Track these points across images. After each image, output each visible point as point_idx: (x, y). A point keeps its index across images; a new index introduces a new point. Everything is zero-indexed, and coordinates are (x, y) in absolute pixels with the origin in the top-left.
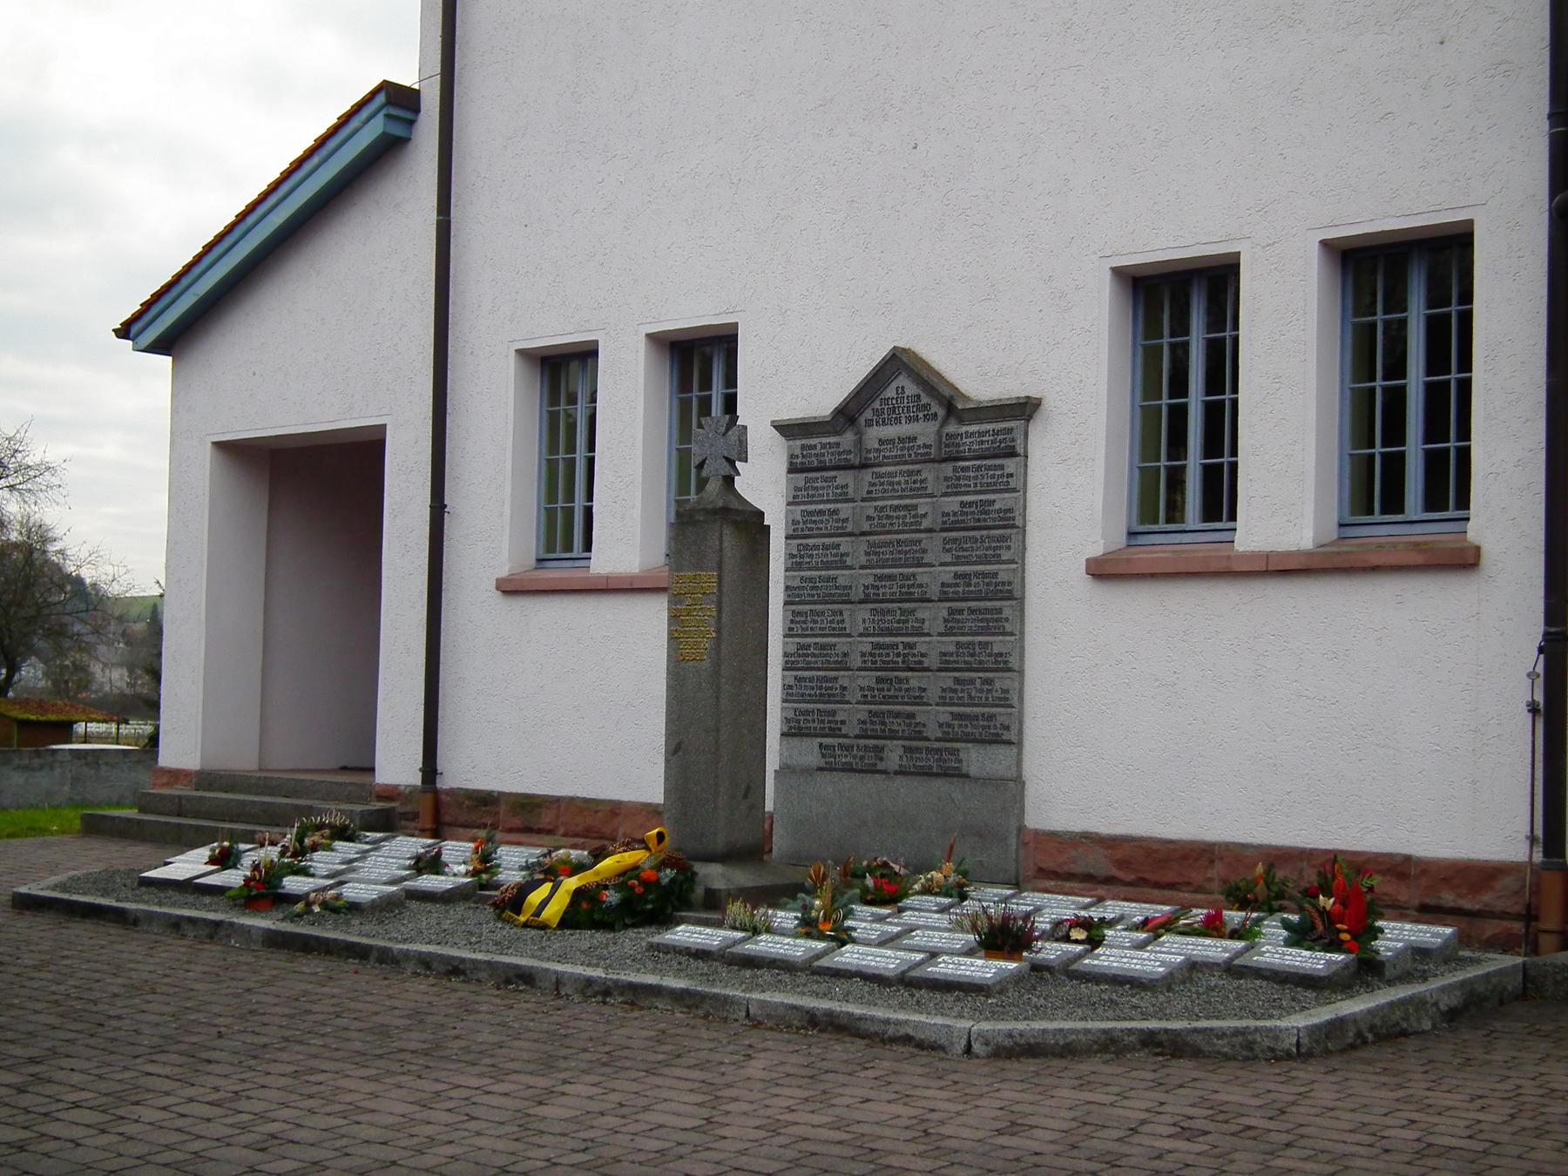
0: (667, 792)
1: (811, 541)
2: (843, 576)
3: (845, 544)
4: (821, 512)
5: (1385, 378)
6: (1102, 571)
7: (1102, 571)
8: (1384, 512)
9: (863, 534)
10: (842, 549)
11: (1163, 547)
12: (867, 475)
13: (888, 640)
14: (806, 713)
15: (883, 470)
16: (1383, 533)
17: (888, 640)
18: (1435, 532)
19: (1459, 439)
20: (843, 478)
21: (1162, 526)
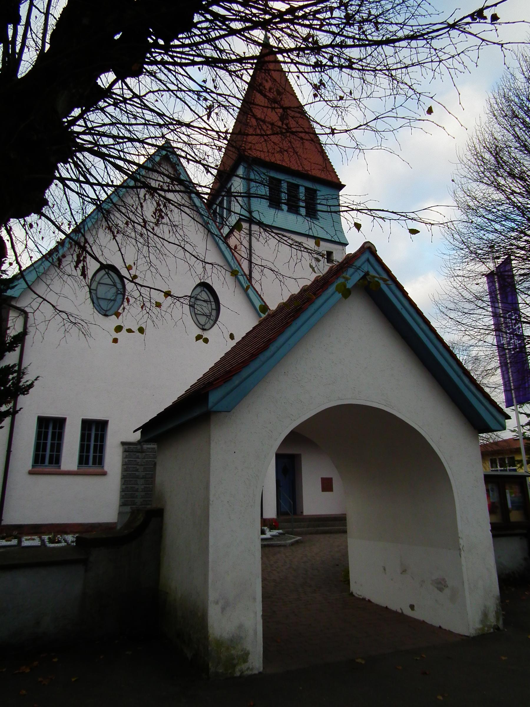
0: (306, 516)
1: (129, 466)
2: (137, 473)
3: (138, 467)
4: (132, 460)
5: (55, 443)
6: (31, 473)
7: (31, 473)
8: (41, 464)
9: (142, 465)
10: (138, 468)
11: (39, 469)
12: (144, 454)
13: (148, 486)
14: (127, 501)
15: (147, 453)
16: (85, 469)
17: (148, 486)
18: (97, 469)
19: (96, 456)
20: (138, 454)
21: (40, 465)
